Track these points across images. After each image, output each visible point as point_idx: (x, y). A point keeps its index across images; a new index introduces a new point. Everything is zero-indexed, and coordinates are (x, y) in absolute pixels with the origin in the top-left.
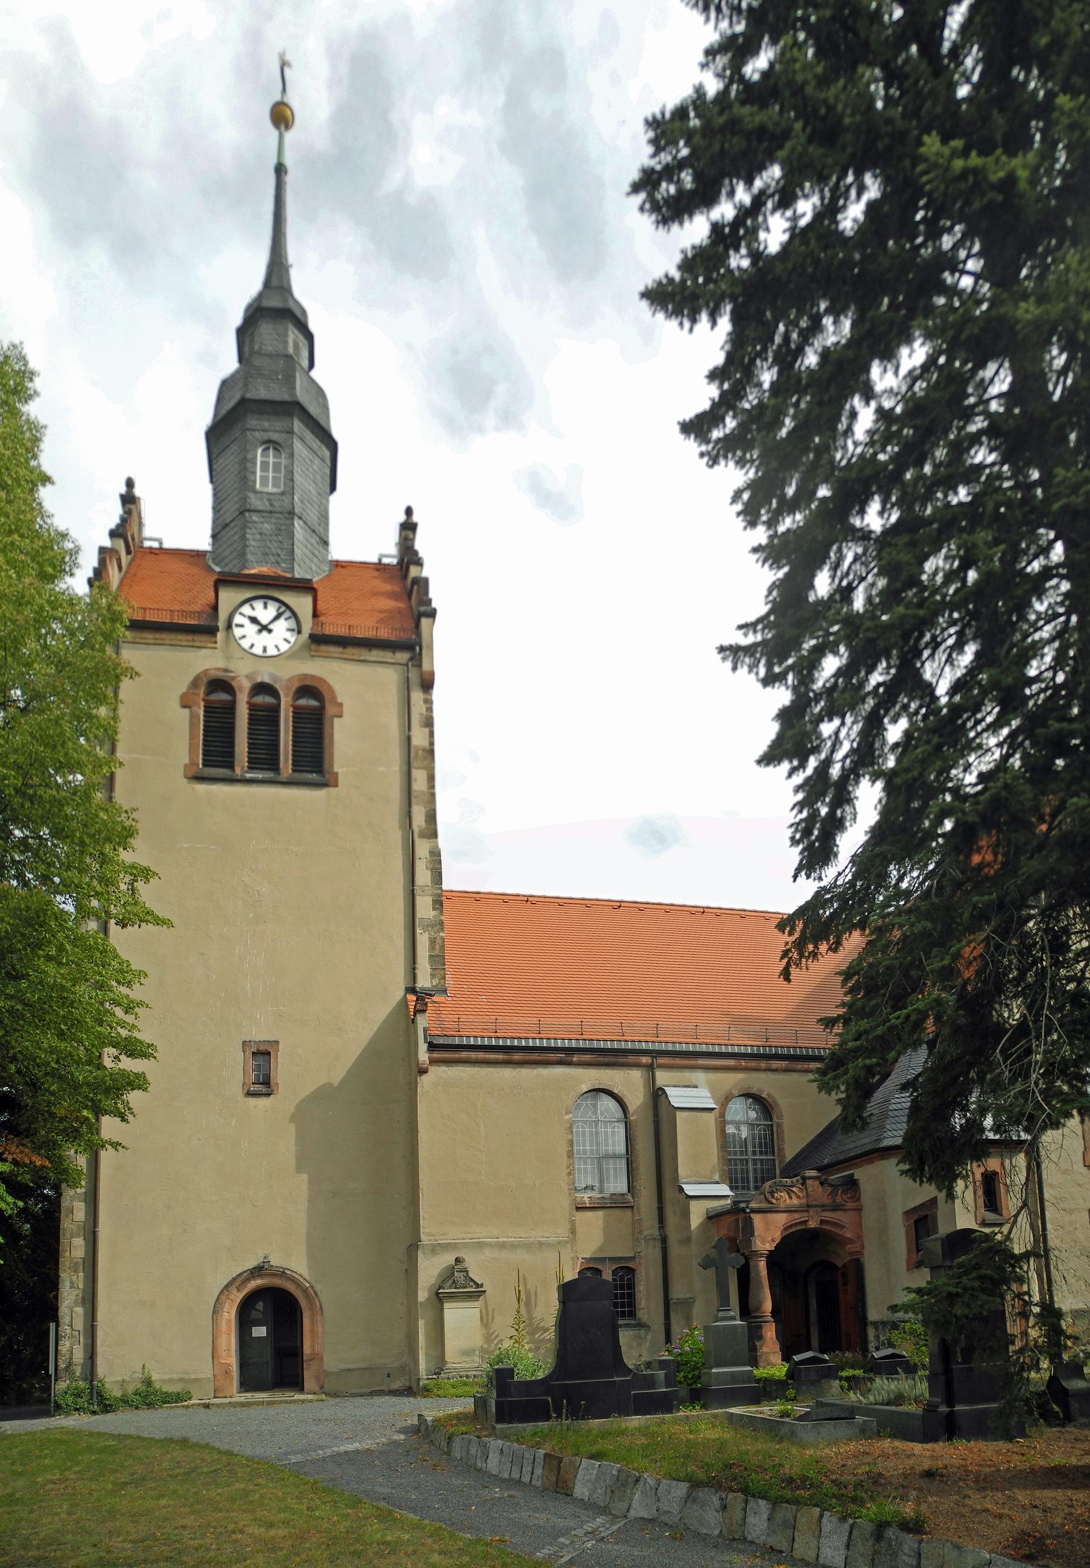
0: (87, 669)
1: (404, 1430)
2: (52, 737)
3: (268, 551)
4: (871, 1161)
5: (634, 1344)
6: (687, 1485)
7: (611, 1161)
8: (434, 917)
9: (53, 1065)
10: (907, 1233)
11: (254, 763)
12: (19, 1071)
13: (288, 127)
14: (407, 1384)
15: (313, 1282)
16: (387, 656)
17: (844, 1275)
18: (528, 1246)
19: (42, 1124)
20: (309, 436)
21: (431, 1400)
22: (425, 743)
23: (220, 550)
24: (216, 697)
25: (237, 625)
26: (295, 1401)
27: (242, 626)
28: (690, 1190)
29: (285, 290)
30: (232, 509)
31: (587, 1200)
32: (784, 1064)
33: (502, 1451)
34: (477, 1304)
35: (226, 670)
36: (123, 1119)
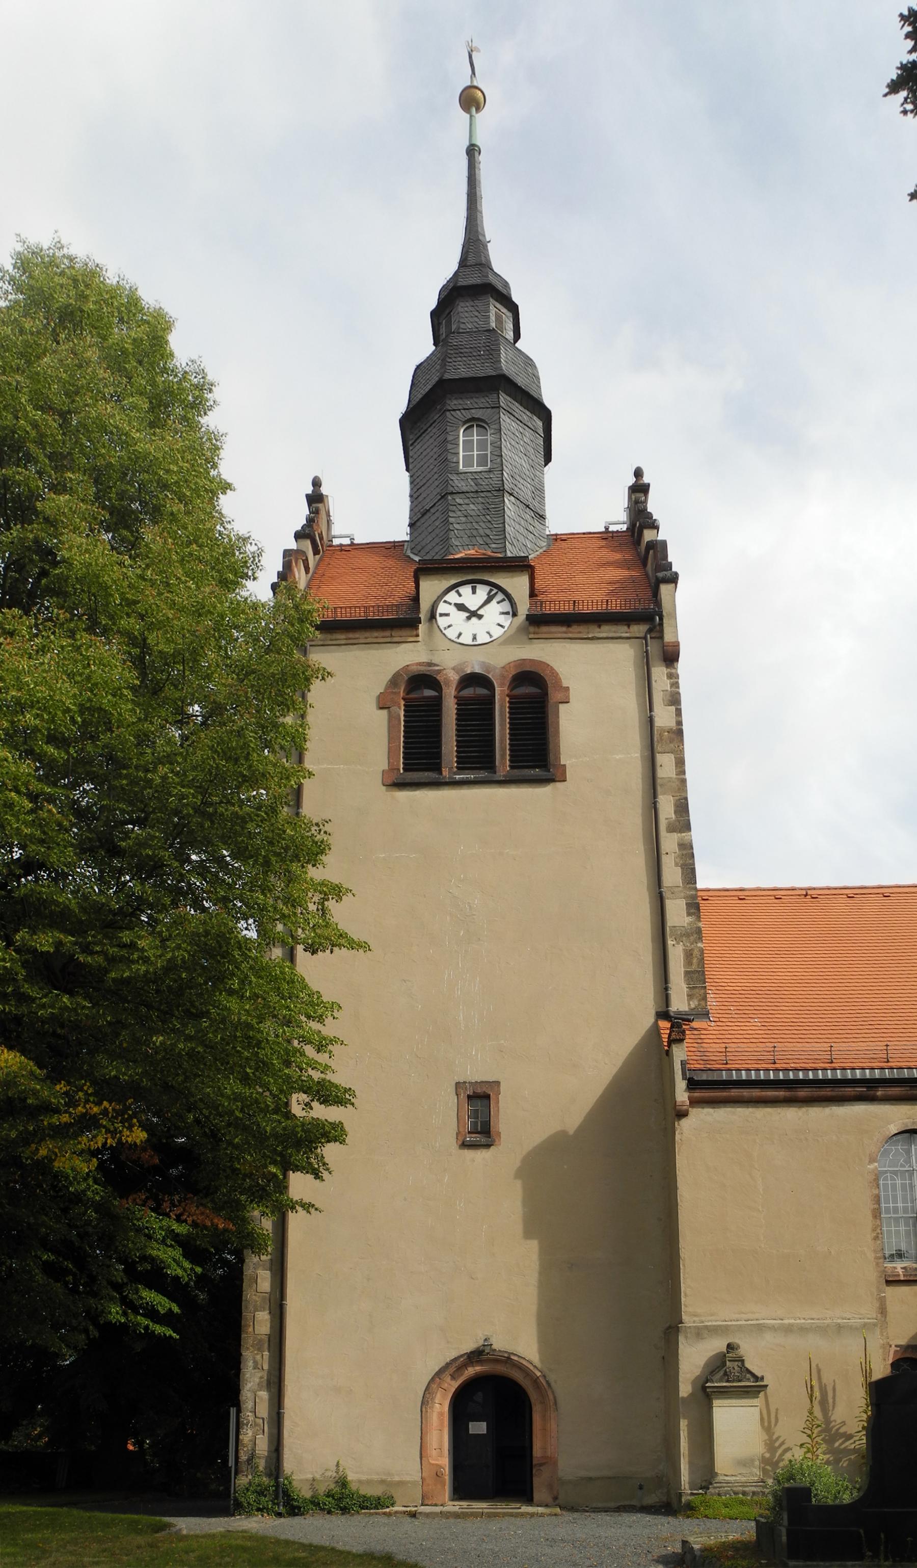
0: (273, 675)
2: (234, 749)
3: (475, 533)
8: (689, 924)
9: (237, 1113)
11: (464, 763)
12: (197, 1121)
13: (478, 109)
14: (664, 1499)
16: (622, 631)
18: (822, 1330)
19: (224, 1181)
20: (517, 408)
21: (696, 1521)
22: (672, 724)
23: (419, 539)
24: (418, 697)
25: (441, 615)
26: (522, 1515)
27: (447, 615)
29: (485, 265)
30: (432, 495)
31: (900, 1271)
34: (755, 1402)
35: (430, 664)
36: (317, 1175)
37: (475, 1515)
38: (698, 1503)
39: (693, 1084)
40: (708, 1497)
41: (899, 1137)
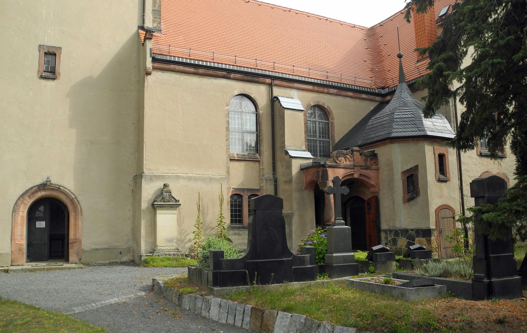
1: (144, 289)
4: (385, 144)
6: (355, 329)
7: (249, 135)
10: (403, 183)
14: (131, 258)
17: (369, 204)
18: (204, 180)
26: (65, 268)
28: (292, 153)
32: (335, 91)
33: (220, 306)
34: (175, 212)
37: (40, 270)
38: (149, 259)
39: (154, 60)
40: (154, 257)
41: (238, 97)
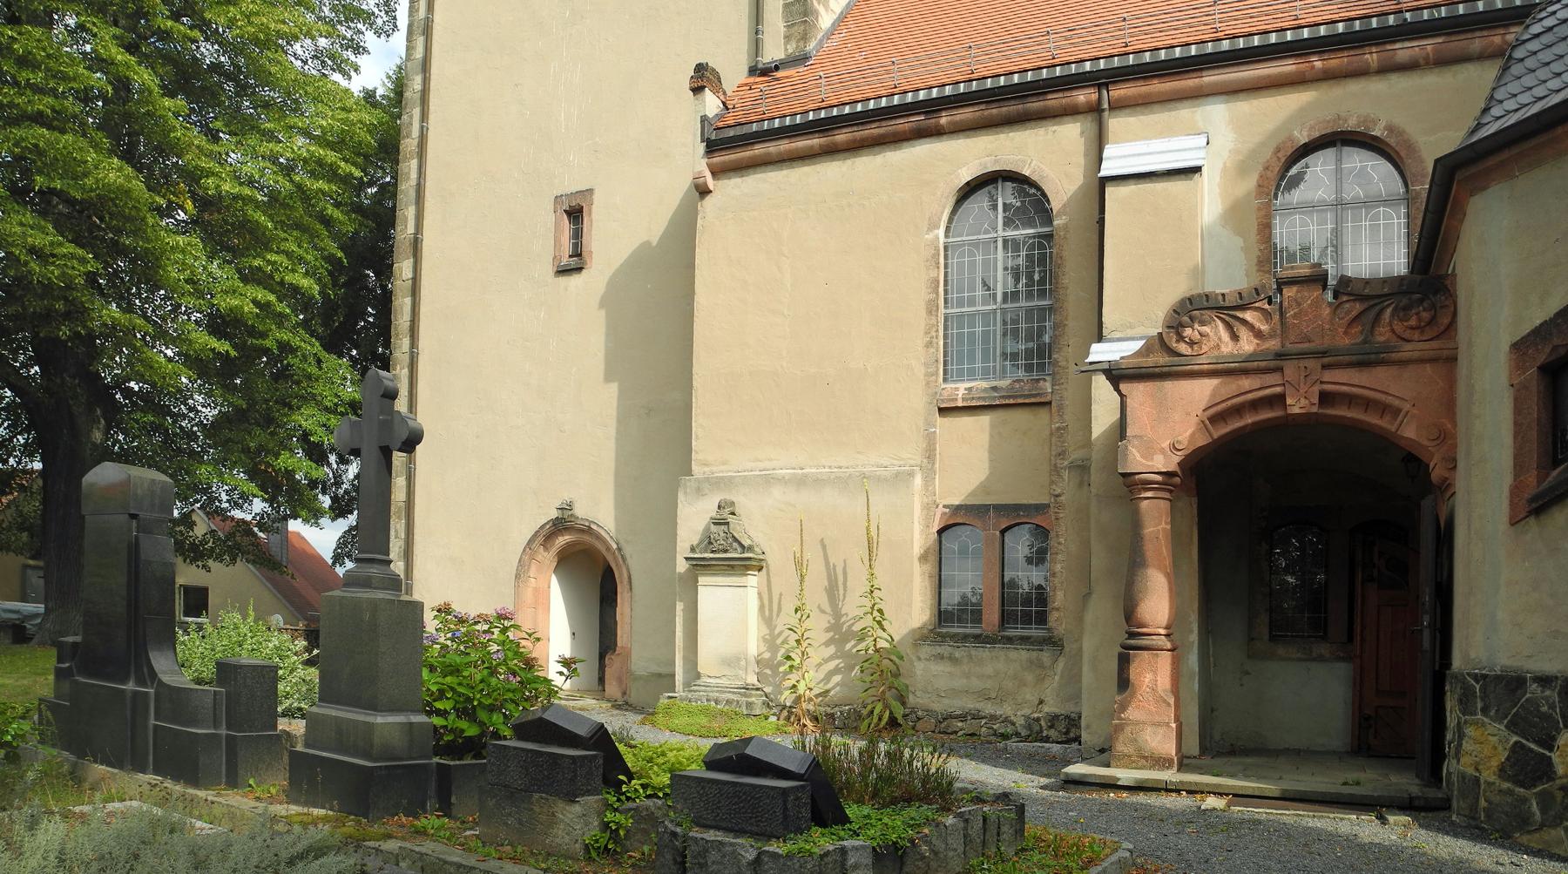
5: (1029, 677)
10: (1518, 410)
15: (622, 542)
